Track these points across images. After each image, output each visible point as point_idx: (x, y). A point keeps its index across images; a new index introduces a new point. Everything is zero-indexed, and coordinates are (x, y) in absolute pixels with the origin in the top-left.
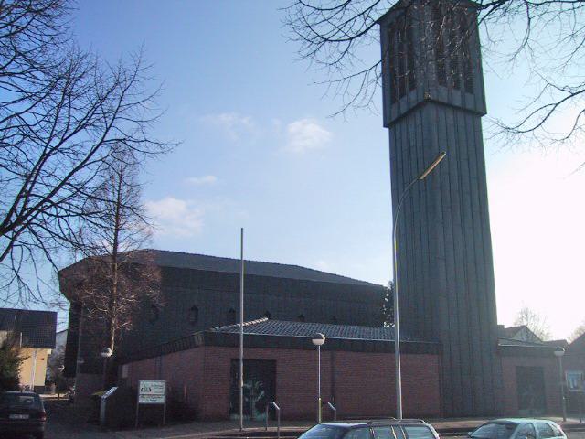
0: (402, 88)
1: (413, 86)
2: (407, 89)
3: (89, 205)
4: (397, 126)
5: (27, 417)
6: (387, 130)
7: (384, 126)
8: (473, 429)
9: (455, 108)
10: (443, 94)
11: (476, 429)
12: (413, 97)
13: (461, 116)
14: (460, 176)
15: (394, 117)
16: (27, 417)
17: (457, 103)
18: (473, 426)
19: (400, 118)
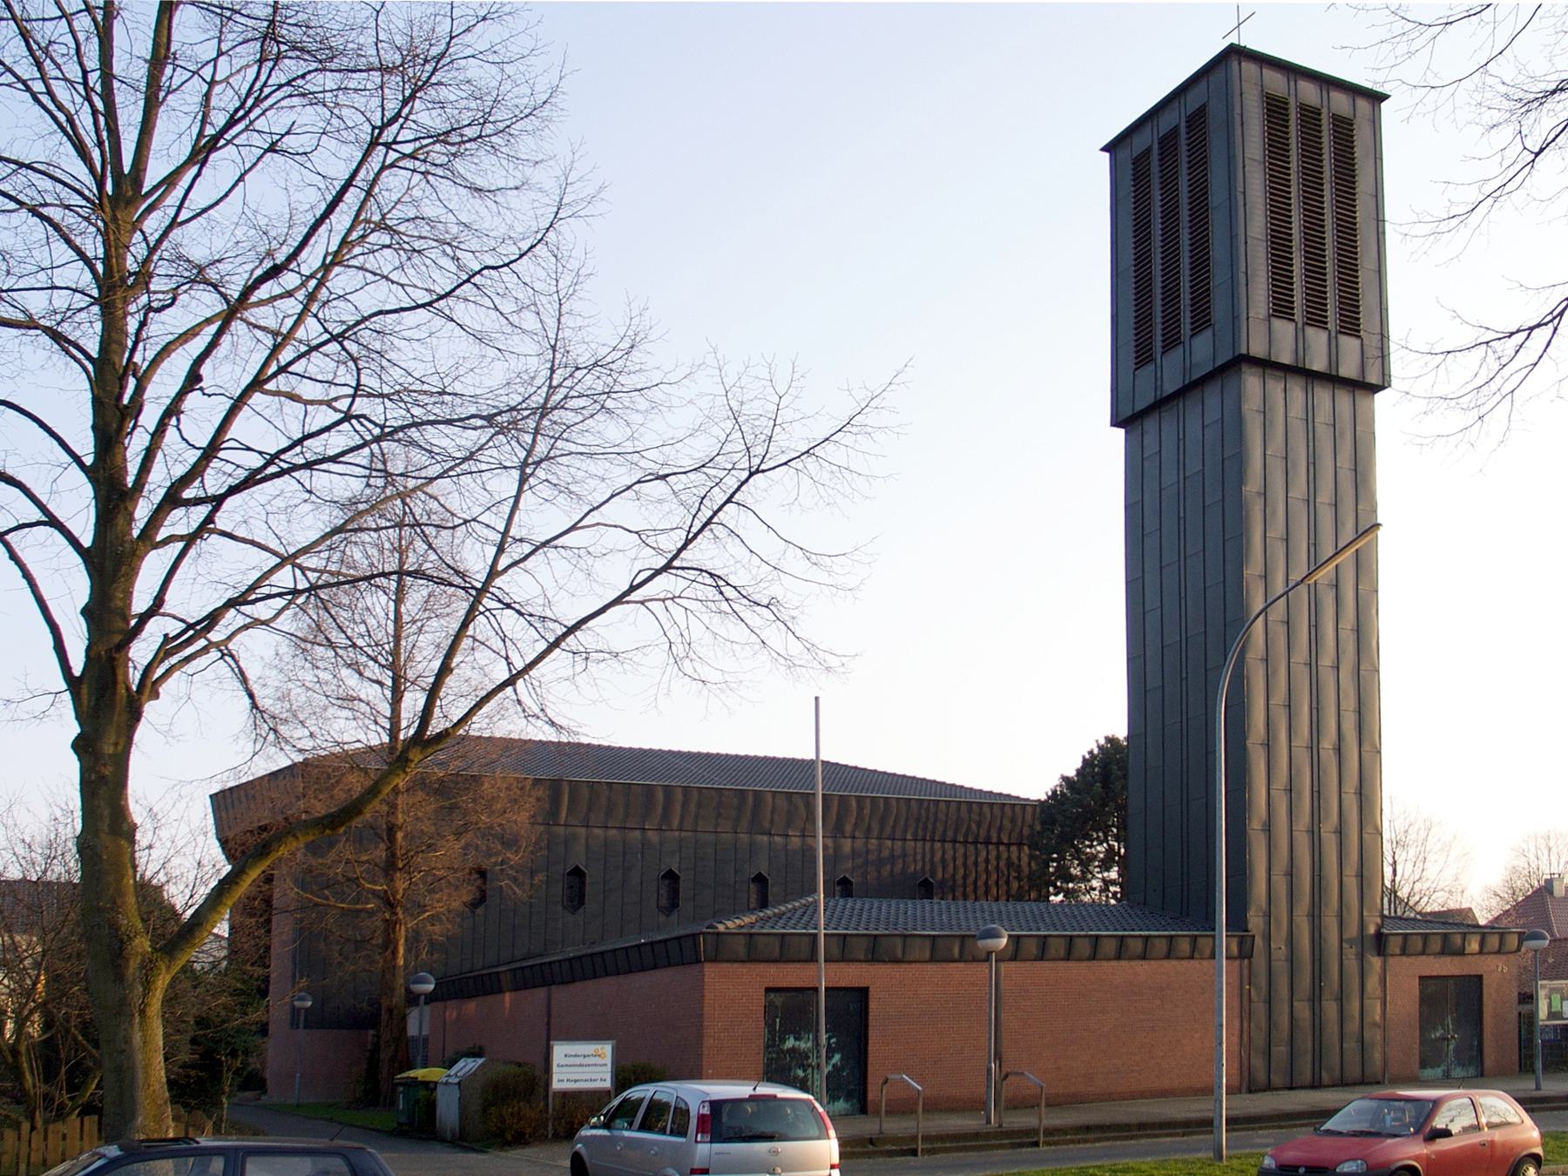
0: (1172, 320)
1: (1202, 320)
2: (1186, 328)
3: (184, 802)
4: (1150, 424)
5: (126, 401)
6: (1122, 431)
7: (1116, 423)
8: (1329, 1113)
9: (1312, 377)
10: (1282, 340)
11: (1336, 1111)
12: (1202, 351)
13: (1323, 395)
14: (1315, 627)
15: (1145, 399)
16: (126, 401)
17: (1318, 364)
18: (1330, 1106)
19: (1160, 404)
